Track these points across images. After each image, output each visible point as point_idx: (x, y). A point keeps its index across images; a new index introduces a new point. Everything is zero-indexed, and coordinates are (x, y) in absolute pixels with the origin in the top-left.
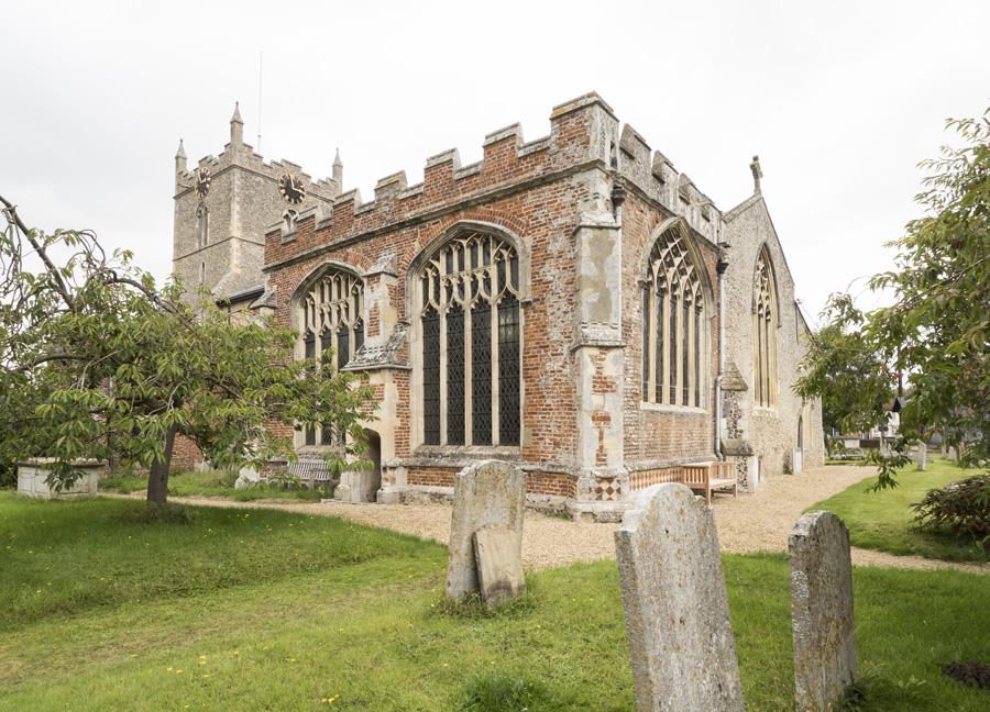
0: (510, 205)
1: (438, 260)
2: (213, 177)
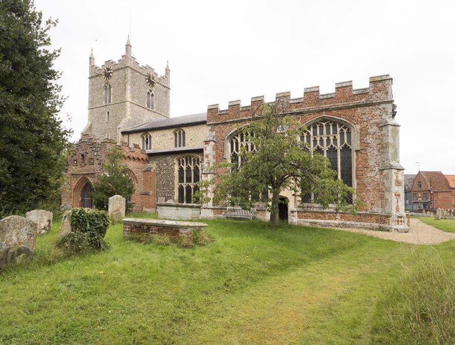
0: (349, 112)
1: (310, 130)
2: (114, 71)
